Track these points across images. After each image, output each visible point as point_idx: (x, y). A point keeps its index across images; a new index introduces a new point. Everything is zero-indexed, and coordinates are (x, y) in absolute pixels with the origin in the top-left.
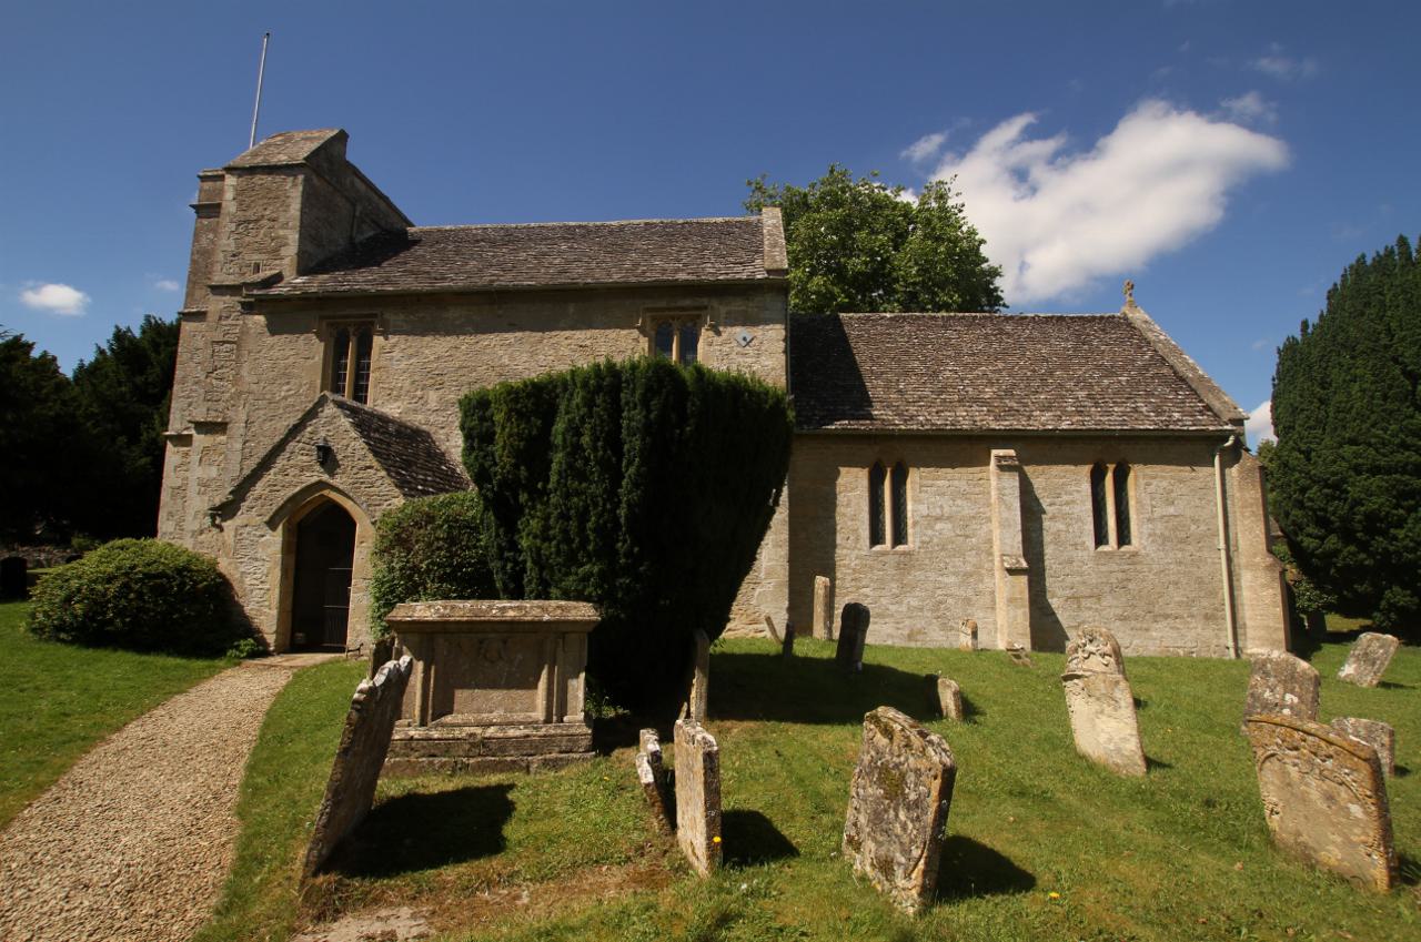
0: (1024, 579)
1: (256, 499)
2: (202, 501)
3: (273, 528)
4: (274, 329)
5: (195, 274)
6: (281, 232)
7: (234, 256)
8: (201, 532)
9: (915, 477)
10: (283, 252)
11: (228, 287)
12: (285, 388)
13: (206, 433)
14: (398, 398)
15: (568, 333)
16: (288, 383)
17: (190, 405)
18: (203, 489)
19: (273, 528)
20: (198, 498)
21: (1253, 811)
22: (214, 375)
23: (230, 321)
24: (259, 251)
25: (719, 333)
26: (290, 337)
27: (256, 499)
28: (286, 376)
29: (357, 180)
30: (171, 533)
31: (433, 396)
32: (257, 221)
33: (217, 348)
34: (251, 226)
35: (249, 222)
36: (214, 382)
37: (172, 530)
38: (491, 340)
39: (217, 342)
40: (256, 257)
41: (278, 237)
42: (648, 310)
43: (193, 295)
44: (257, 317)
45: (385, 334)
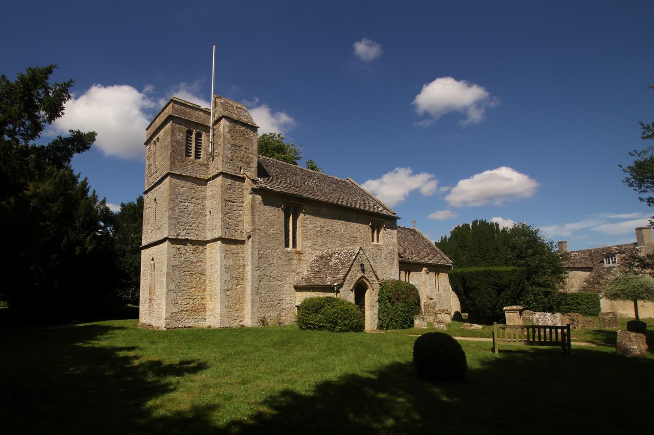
0: (640, 303)
1: (348, 281)
2: (228, 276)
3: (352, 291)
4: (266, 203)
5: (175, 153)
6: (250, 156)
7: (231, 160)
8: (228, 290)
9: (440, 273)
10: (252, 165)
11: (229, 175)
12: (272, 229)
13: (226, 244)
14: (309, 239)
15: (354, 224)
16: (273, 227)
17: (179, 222)
18: (227, 270)
19: (352, 291)
20: (225, 274)
21: (252, 346)
22: (227, 216)
23: (230, 191)
24: (242, 161)
25: (385, 230)
26: (272, 208)
27: (348, 281)
28: (272, 224)
29: (197, 113)
30: (174, 290)
31: (320, 240)
32: (240, 147)
33: (227, 203)
34: (237, 148)
35: (236, 146)
36: (228, 220)
37: (174, 288)
38: (335, 222)
39: (227, 201)
40: (240, 164)
41: (249, 157)
42: (372, 220)
43: (174, 164)
44: (258, 196)
45: (305, 214)
